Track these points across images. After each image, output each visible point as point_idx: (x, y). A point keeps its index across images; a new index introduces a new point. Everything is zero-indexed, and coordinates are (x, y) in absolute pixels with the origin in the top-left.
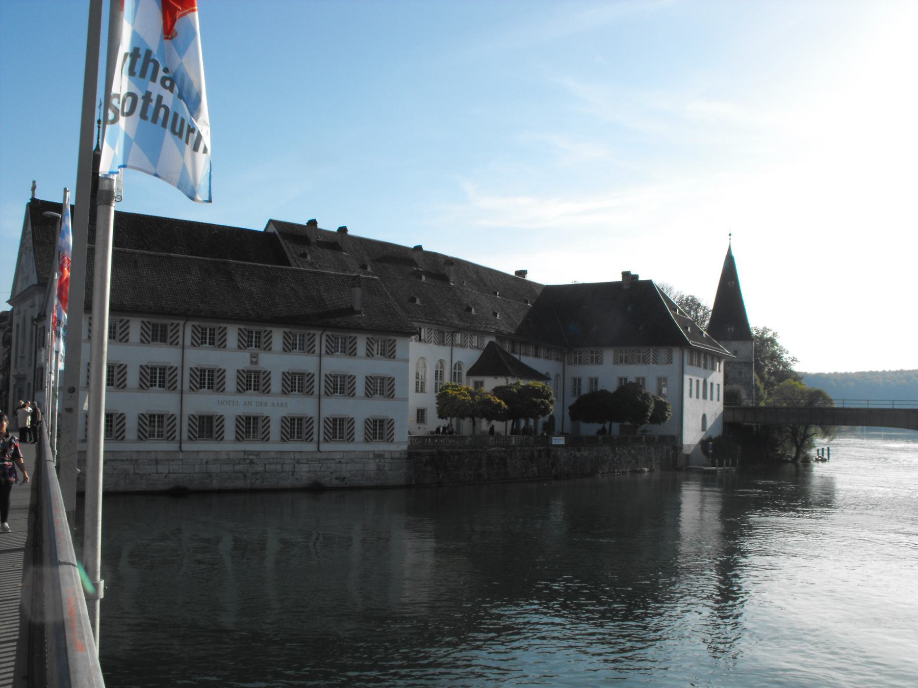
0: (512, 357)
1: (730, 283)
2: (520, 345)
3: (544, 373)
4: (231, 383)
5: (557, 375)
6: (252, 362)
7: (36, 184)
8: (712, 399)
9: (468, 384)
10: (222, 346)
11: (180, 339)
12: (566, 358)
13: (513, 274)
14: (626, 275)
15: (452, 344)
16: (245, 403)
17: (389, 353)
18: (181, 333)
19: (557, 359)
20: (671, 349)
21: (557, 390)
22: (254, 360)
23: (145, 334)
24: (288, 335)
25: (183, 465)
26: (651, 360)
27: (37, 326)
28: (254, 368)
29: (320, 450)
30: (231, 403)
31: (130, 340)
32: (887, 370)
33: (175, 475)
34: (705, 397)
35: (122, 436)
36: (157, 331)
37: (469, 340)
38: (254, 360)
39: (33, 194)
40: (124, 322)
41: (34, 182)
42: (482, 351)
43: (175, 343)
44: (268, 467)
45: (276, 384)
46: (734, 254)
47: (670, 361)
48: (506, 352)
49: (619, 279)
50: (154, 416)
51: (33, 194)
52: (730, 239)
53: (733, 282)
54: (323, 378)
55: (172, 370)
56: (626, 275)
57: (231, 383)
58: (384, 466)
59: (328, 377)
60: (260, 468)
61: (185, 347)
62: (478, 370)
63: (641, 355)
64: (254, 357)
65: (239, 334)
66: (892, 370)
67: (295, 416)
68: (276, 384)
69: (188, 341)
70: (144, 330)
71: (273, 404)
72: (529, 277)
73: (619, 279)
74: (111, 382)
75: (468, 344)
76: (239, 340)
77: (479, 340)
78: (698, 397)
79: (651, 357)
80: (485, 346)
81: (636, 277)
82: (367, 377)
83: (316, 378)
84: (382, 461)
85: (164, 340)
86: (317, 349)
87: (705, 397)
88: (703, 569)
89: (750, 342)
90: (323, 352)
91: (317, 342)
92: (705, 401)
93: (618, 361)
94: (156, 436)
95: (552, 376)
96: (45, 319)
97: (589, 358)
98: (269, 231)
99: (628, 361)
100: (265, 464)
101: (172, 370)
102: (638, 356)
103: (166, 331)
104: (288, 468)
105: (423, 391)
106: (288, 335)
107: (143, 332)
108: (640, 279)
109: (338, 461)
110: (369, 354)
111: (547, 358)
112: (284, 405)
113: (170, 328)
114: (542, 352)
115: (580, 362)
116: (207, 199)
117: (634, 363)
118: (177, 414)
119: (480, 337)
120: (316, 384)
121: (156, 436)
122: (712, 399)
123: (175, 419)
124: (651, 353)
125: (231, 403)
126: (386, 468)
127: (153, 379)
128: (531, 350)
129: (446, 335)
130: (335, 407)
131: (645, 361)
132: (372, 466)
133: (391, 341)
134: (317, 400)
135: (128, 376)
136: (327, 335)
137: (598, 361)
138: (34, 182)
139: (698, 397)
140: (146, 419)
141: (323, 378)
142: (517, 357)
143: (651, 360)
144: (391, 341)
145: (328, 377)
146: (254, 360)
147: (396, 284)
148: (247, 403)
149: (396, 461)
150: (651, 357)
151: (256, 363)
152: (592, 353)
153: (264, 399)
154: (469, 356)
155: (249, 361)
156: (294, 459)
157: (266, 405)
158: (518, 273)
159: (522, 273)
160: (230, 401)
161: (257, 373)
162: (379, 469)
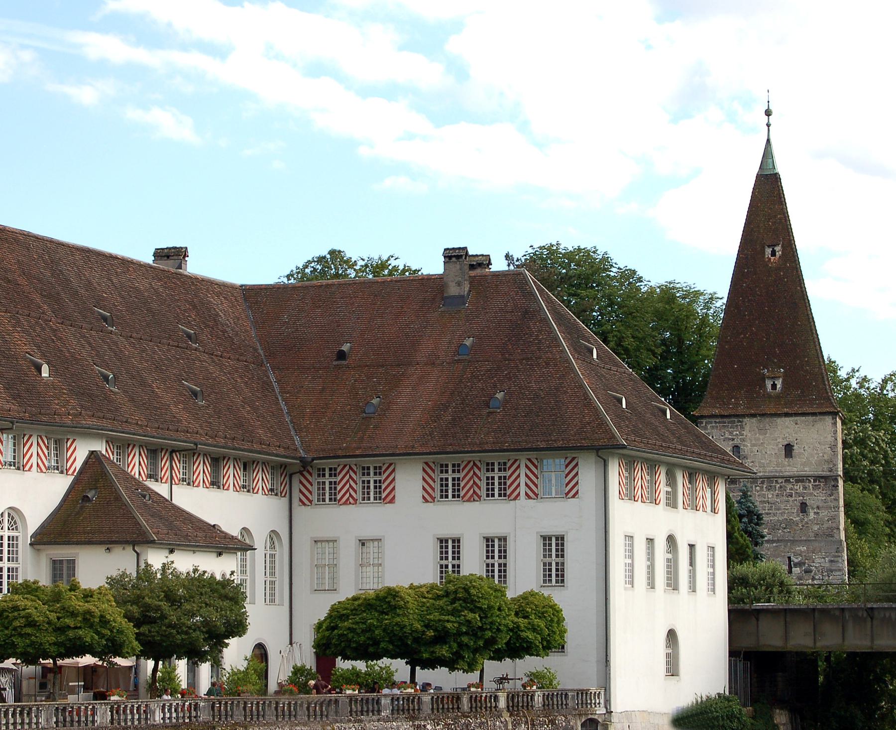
0: (149, 489)
2: (172, 459)
3: (235, 532)
8: (693, 588)
13: (148, 259)
14: (453, 256)
20: (573, 459)
21: (273, 574)
26: (523, 489)
29: (293, 476)
34: (673, 584)
42: (71, 479)
46: (782, 167)
47: (571, 492)
48: (133, 478)
52: (768, 125)
53: (778, 248)
56: (453, 256)
72: (194, 267)
73: (434, 266)
78: (651, 584)
79: (523, 479)
80: (78, 464)
87: (673, 584)
92: (673, 596)
95: (259, 540)
97: (359, 487)
99: (462, 493)
102: (442, 479)
111: (247, 488)
114: (231, 474)
117: (475, 497)
122: (693, 588)
127: (444, 469)
128: (202, 470)
131: (506, 493)
139: (651, 584)
142: (161, 489)
143: (523, 489)
150: (523, 479)
152: (490, 467)
158: (161, 254)
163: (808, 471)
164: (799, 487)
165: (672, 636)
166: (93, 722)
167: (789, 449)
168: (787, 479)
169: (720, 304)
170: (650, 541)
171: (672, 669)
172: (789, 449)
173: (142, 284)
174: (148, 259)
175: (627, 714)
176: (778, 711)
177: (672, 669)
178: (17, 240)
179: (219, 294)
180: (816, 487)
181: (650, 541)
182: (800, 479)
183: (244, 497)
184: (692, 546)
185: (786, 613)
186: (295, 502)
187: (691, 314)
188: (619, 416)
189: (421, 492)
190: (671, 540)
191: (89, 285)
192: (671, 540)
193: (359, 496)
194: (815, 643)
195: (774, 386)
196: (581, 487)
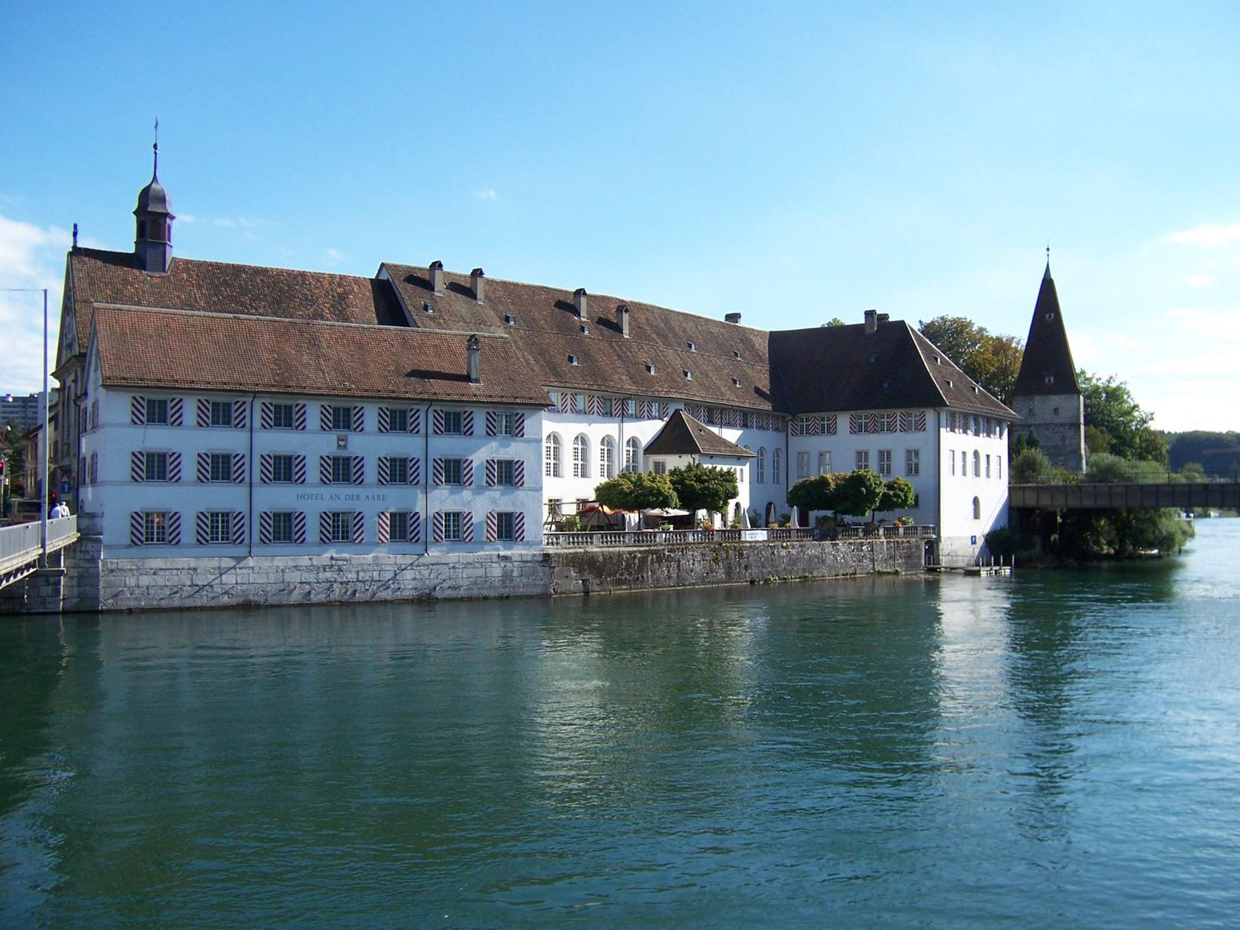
1: (1047, 316)
4: (313, 472)
5: (777, 451)
6: (339, 446)
7: (78, 228)
9: (646, 466)
10: (300, 428)
11: (247, 420)
12: (790, 427)
13: (723, 320)
14: (869, 314)
15: (623, 414)
16: (332, 497)
17: (514, 430)
18: (247, 413)
19: (777, 429)
22: (342, 443)
23: (202, 415)
24: (267, 407)
25: (254, 573)
27: (79, 406)
28: (343, 453)
30: (314, 497)
31: (184, 423)
32: (1173, 432)
33: (244, 587)
35: (177, 539)
36: (219, 411)
37: (646, 408)
38: (342, 443)
39: (75, 241)
40: (176, 401)
41: (75, 226)
42: (664, 423)
43: (240, 425)
44: (361, 574)
45: (371, 472)
49: (861, 320)
50: (217, 515)
51: (75, 241)
53: (1052, 314)
54: (431, 463)
55: (299, 459)
56: (869, 314)
57: (313, 472)
58: (512, 571)
59: (436, 462)
60: (352, 576)
61: (254, 430)
62: (657, 446)
63: (913, 419)
64: (342, 440)
65: (380, 415)
66: (1178, 432)
67: (280, 511)
68: (371, 472)
69: (257, 422)
70: (201, 410)
71: (367, 497)
72: (742, 323)
73: (861, 320)
74: (277, 476)
75: (646, 413)
76: (379, 422)
77: (638, 407)
81: (885, 316)
82: (133, 454)
83: (422, 464)
84: (509, 565)
85: (227, 422)
86: (422, 428)
88: (1126, 706)
89: (1075, 396)
90: (430, 431)
91: (422, 420)
93: (856, 429)
94: (155, 539)
96: (86, 398)
98: (382, 277)
100: (358, 572)
101: (299, 459)
103: (229, 411)
104: (389, 575)
105: (778, 482)
106: (267, 407)
107: (134, 410)
108: (890, 320)
109: (451, 566)
110: (491, 433)
111: (761, 428)
112: (381, 498)
113: (170, 405)
115: (802, 432)
116: (126, 243)
118: (246, 511)
119: (661, 405)
120: (422, 471)
121: (155, 539)
123: (243, 517)
124: (755, 419)
125: (314, 497)
126: (515, 574)
129: (614, 402)
130: (226, 497)
132: (497, 571)
133: (519, 416)
134: (247, 490)
135: (184, 466)
136: (435, 411)
137: (831, 430)
138: (75, 226)
140: (142, 518)
141: (431, 463)
144: (519, 416)
145: (436, 462)
146: (342, 443)
147: (547, 340)
148: (334, 497)
149: (529, 564)
150: (898, 422)
151: (345, 447)
152: (823, 419)
153: (300, 490)
154: (648, 430)
155: (336, 445)
156: (396, 564)
157: (358, 497)
158: (729, 317)
159: (734, 317)
160: (312, 495)
161: (347, 459)
162: (507, 576)
163: (1066, 421)
164: (1061, 429)
165: (976, 501)
166: (655, 541)
167: (1056, 410)
168: (1056, 425)
169: (1024, 342)
170: (964, 453)
171: (976, 516)
172: (1056, 410)
173: (715, 330)
174: (723, 320)
175: (949, 538)
176: (761, 620)
177: (976, 516)
178: (647, 309)
179: (756, 336)
180: (1069, 429)
181: (964, 453)
182: (1062, 425)
183: (761, 432)
184: (988, 456)
185: (1024, 491)
186: (789, 435)
187: (1010, 348)
188: (947, 391)
189: (849, 429)
190: (976, 454)
191: (684, 330)
192: (976, 454)
193: (819, 431)
194: (1052, 502)
195: (1049, 380)
196: (927, 426)
